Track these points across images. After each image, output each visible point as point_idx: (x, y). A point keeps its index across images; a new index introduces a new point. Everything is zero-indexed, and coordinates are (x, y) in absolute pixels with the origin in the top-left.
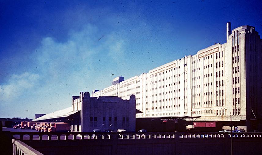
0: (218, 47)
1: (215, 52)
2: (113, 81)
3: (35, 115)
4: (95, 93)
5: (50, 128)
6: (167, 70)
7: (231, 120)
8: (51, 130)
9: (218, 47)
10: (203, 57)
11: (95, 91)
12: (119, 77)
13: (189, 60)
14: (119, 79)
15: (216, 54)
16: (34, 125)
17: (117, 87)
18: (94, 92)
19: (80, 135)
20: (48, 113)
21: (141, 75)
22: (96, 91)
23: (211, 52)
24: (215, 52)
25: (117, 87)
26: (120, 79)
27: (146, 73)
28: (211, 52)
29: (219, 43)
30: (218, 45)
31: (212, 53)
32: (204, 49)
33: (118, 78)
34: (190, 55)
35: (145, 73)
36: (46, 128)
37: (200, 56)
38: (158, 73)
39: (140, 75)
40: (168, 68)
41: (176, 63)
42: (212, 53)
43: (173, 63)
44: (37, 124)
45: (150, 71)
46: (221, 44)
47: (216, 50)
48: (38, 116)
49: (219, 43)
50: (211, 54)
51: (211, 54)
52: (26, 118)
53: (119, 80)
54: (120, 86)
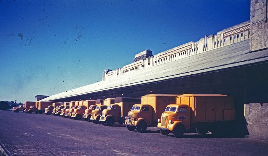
0: (191, 45)
1: (188, 49)
3: (36, 97)
4: (109, 73)
5: (48, 108)
6: (162, 59)
7: (83, 104)
9: (191, 45)
10: (229, 36)
11: (107, 70)
12: (146, 51)
14: (146, 53)
15: (230, 38)
16: (49, 106)
17: (118, 72)
18: (106, 72)
20: (52, 95)
22: (109, 70)
24: (188, 49)
25: (118, 72)
26: (148, 54)
27: (121, 68)
28: (185, 49)
29: (193, 42)
30: (192, 43)
33: (145, 53)
35: (120, 68)
36: (59, 108)
37: (226, 35)
38: (135, 67)
40: (136, 65)
41: (193, 45)
44: (56, 105)
45: (124, 67)
46: (194, 42)
47: (189, 47)
48: (39, 97)
49: (193, 42)
50: (186, 51)
51: (241, 32)
52: (19, 103)
53: (146, 54)
54: (121, 71)
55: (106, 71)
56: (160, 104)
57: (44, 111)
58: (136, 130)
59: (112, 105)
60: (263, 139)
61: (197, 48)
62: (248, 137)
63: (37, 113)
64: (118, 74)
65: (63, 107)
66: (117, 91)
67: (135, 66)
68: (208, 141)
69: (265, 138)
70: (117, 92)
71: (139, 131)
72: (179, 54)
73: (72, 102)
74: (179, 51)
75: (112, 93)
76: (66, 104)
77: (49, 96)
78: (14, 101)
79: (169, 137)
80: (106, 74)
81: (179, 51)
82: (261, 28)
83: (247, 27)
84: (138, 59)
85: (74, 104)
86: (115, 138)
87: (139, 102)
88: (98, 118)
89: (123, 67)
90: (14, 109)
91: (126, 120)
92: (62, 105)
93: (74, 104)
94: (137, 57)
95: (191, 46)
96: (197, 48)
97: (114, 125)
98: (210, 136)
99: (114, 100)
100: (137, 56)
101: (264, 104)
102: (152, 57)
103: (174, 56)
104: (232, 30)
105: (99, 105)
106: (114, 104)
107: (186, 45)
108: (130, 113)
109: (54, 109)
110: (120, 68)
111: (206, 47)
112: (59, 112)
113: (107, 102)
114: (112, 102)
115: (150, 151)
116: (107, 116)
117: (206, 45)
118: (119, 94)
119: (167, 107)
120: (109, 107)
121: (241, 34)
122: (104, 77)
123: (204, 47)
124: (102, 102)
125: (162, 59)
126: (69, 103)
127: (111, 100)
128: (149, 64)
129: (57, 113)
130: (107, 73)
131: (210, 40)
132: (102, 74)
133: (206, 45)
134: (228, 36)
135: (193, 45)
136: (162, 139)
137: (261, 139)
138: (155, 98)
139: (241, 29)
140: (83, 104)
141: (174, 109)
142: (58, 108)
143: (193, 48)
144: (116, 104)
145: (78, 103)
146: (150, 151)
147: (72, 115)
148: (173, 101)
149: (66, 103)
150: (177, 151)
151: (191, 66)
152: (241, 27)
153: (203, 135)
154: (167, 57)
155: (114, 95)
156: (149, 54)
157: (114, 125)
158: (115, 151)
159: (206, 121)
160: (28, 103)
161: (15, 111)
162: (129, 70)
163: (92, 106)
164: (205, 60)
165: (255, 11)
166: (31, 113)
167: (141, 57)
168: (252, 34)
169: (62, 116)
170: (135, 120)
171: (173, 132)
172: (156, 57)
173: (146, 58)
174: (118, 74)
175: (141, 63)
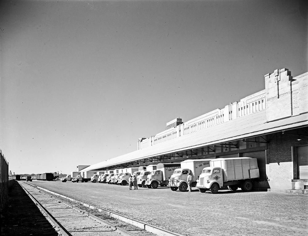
3: (78, 167)
4: (143, 141)
18: (140, 140)
22: (143, 139)
26: (178, 121)
33: (175, 121)
37: (248, 102)
43: (251, 97)
45: (157, 135)
55: (141, 139)
56: (197, 168)
58: (178, 190)
59: (155, 171)
60: (282, 191)
62: (270, 190)
63: (83, 182)
64: (152, 141)
65: (107, 175)
66: (156, 158)
68: (238, 195)
69: (283, 190)
70: (156, 159)
71: (181, 190)
73: (116, 170)
75: (152, 160)
76: (109, 172)
78: (57, 173)
79: (207, 194)
80: (140, 142)
82: (275, 103)
84: (170, 126)
85: (117, 172)
86: (164, 197)
87: (179, 166)
88: (144, 182)
89: (156, 134)
90: (63, 179)
91: (170, 182)
92: (106, 174)
93: (117, 172)
94: (168, 125)
97: (158, 188)
98: (239, 191)
99: (156, 166)
100: (168, 124)
101: (281, 163)
102: (182, 124)
104: (253, 97)
105: (143, 172)
106: (156, 169)
107: (213, 112)
108: (173, 176)
109: (99, 177)
110: (153, 137)
111: (231, 113)
112: (104, 180)
113: (150, 168)
114: (155, 168)
115: (195, 204)
116: (152, 180)
117: (231, 112)
118: (158, 160)
119: (204, 169)
120: (152, 173)
122: (139, 145)
123: (229, 114)
124: (145, 168)
126: (180, 164)
127: (153, 166)
128: (180, 131)
129: (102, 180)
130: (141, 141)
131: (234, 106)
132: (137, 143)
133: (231, 112)
134: (250, 103)
135: (218, 112)
136: (202, 195)
137: (281, 191)
138: (193, 163)
139: (249, 101)
140: (127, 172)
141: (209, 171)
142: (102, 176)
144: (158, 169)
145: (121, 171)
146: (195, 204)
147: (118, 181)
148: (208, 164)
150: (215, 202)
151: (221, 134)
152: (262, 94)
153: (234, 191)
155: (153, 162)
156: (179, 122)
157: (158, 188)
158: (169, 204)
159: (236, 180)
160: (74, 173)
163: (136, 172)
164: (231, 128)
165: (269, 89)
166: (78, 182)
167: (172, 125)
168: (268, 108)
169: (108, 183)
170: (178, 182)
171: (210, 189)
172: (186, 124)
173: (177, 125)
174: (152, 141)
175: (173, 131)
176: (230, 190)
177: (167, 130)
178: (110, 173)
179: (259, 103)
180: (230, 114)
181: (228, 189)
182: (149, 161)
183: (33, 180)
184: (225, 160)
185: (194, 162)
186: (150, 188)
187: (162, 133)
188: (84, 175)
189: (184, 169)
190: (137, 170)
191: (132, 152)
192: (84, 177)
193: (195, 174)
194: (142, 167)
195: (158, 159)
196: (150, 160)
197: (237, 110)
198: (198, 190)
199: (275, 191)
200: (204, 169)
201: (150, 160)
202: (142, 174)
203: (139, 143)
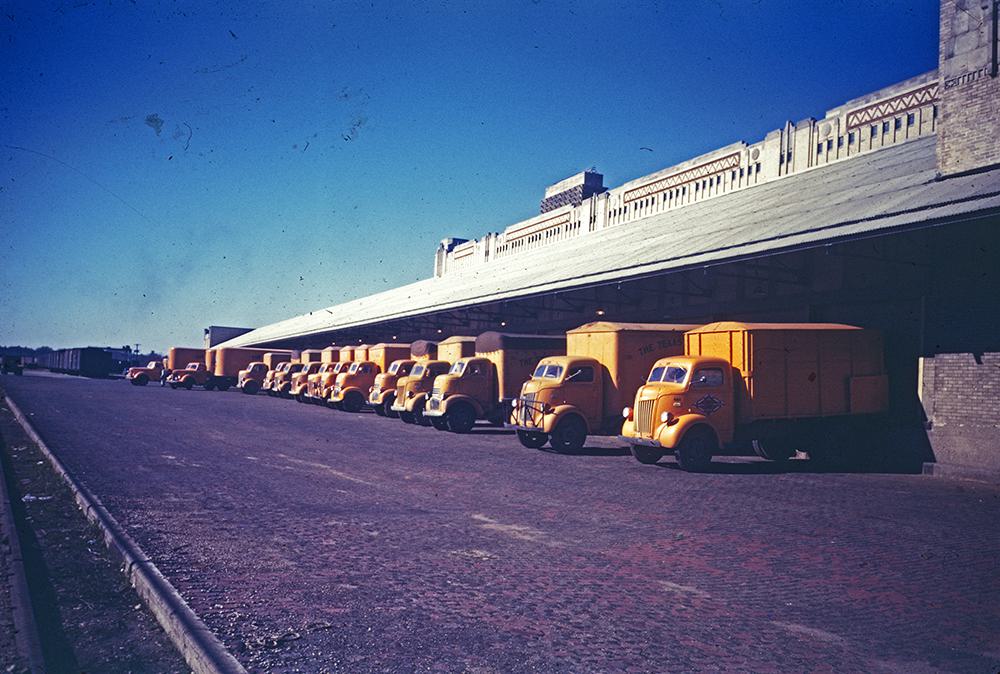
0: (738, 154)
1: (727, 169)
2: (548, 195)
3: (207, 332)
4: (456, 249)
6: (638, 201)
8: (249, 375)
9: (738, 154)
10: (693, 180)
11: (451, 242)
12: (582, 175)
13: (801, 138)
14: (582, 182)
15: (869, 129)
16: (252, 364)
17: (488, 246)
18: (446, 247)
19: (438, 378)
21: (484, 239)
22: (457, 242)
23: (718, 166)
24: (727, 169)
25: (488, 246)
27: (497, 234)
28: (718, 166)
29: (743, 143)
30: (739, 147)
31: (914, 107)
32: (732, 145)
33: (579, 180)
34: (807, 117)
35: (493, 235)
37: (856, 121)
39: (480, 240)
40: (550, 223)
41: (743, 154)
42: (914, 107)
43: (678, 169)
45: (509, 229)
46: (747, 145)
48: (219, 334)
49: (743, 143)
52: (150, 352)
53: (584, 187)
54: (499, 245)
55: (446, 243)
56: (630, 357)
57: (236, 380)
59: (466, 361)
60: (985, 477)
61: (758, 166)
62: (930, 470)
63: (209, 388)
64: (487, 253)
65: (298, 368)
67: (544, 225)
68: (796, 484)
70: (483, 317)
71: (559, 448)
72: (697, 185)
73: (330, 348)
74: (697, 174)
76: (308, 356)
77: (251, 330)
78: (133, 348)
79: (663, 470)
80: (445, 252)
81: (697, 174)
83: (929, 93)
84: (557, 202)
85: (336, 356)
87: (561, 349)
88: (420, 404)
91: (515, 412)
92: (297, 362)
93: (336, 356)
95: (737, 157)
96: (758, 166)
97: (474, 429)
98: (800, 467)
100: (551, 192)
101: (986, 357)
102: (602, 195)
103: (678, 191)
104: (877, 102)
105: (423, 361)
106: (474, 355)
107: (721, 153)
109: (270, 374)
110: (493, 235)
111: (789, 160)
113: (450, 351)
114: (468, 349)
117: (789, 155)
120: (457, 366)
121: (884, 124)
122: (439, 264)
123: (782, 162)
124: (433, 351)
125: (638, 201)
126: (320, 354)
129: (278, 387)
130: (450, 249)
133: (789, 155)
135: (744, 154)
136: (638, 477)
137: (978, 476)
139: (906, 100)
141: (678, 374)
142: (282, 370)
143: (744, 165)
144: (479, 355)
148: (676, 346)
149: (311, 354)
153: (779, 464)
154: (655, 196)
156: (594, 186)
157: (474, 429)
159: (789, 417)
160: (178, 352)
161: (134, 381)
162: (526, 239)
163: (399, 363)
167: (567, 196)
172: (617, 197)
174: (487, 253)
175: (566, 217)
176: (763, 456)
177: (545, 215)
178: (311, 361)
179: (908, 124)
180: (784, 167)
181: (753, 453)
182: (456, 322)
183: (25, 372)
184: (749, 332)
185: (618, 332)
186: (445, 428)
187: (665, 174)
188: (213, 362)
189: (574, 359)
190: (406, 353)
191: (371, 294)
192: (214, 369)
193: (619, 383)
194: (425, 343)
195: (490, 314)
196: (460, 319)
197: (605, 218)
198: (628, 448)
199: (953, 474)
200: (545, 362)
201: (460, 319)
202: (306, 369)
203: (440, 258)
